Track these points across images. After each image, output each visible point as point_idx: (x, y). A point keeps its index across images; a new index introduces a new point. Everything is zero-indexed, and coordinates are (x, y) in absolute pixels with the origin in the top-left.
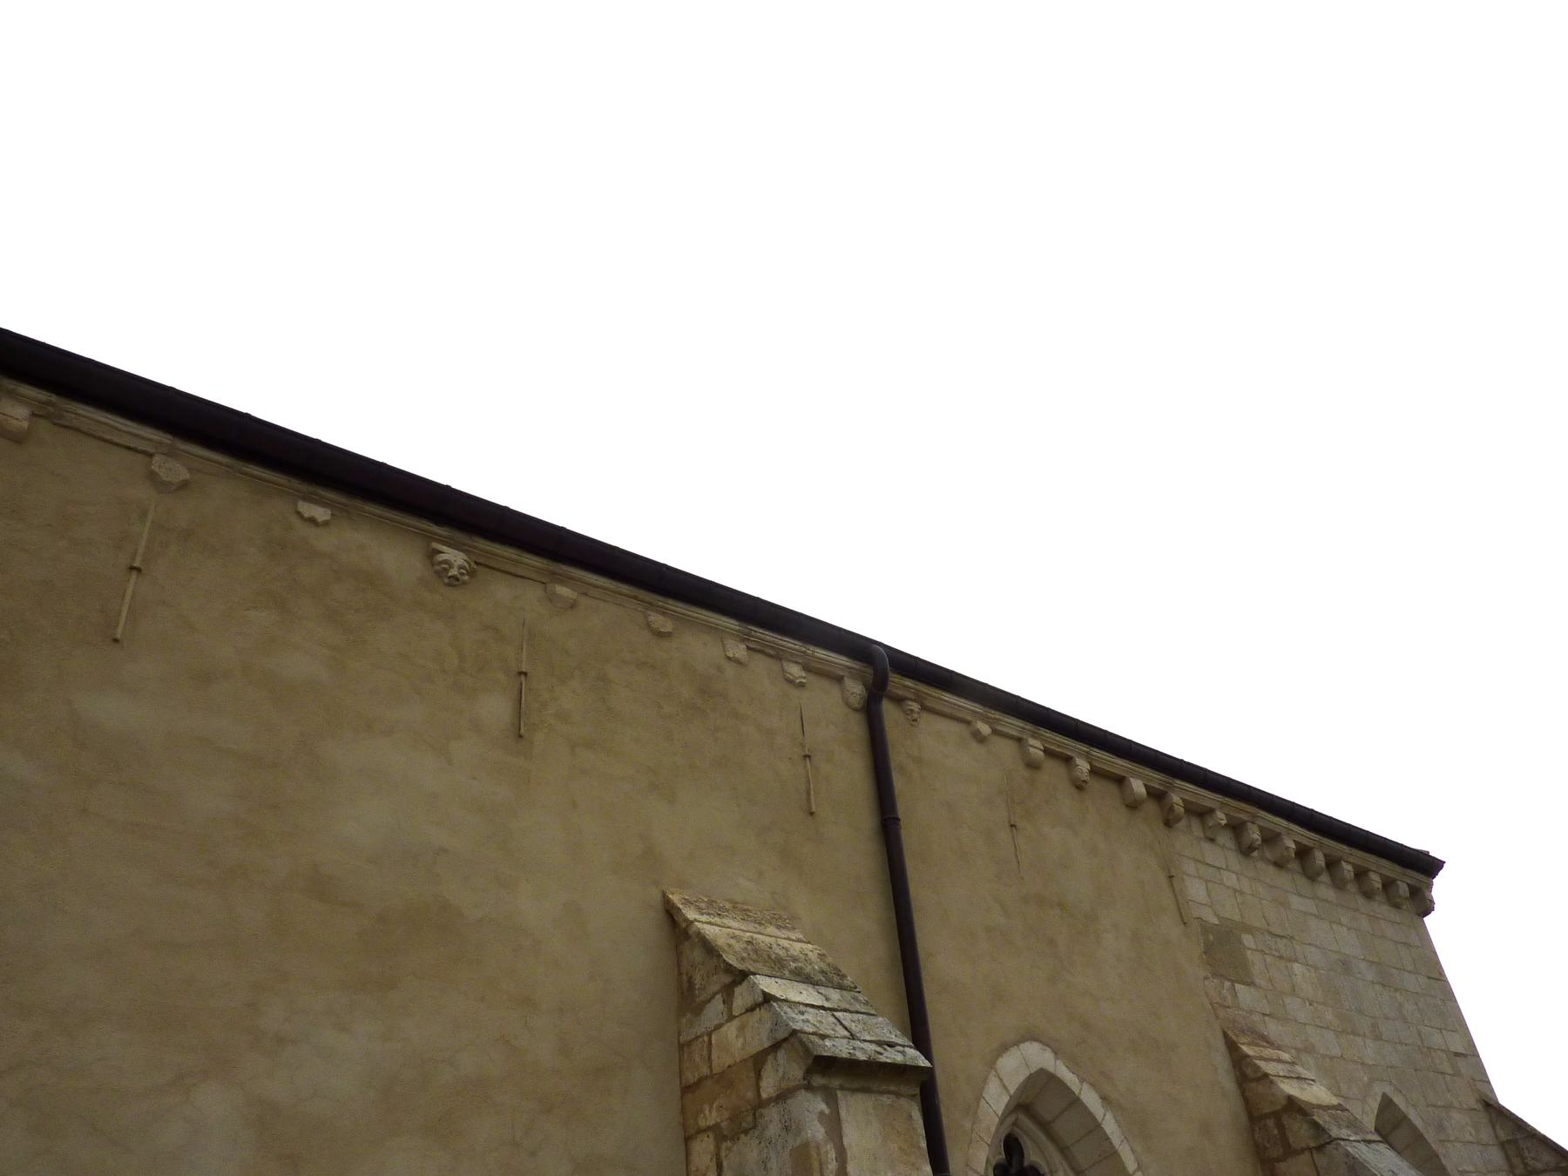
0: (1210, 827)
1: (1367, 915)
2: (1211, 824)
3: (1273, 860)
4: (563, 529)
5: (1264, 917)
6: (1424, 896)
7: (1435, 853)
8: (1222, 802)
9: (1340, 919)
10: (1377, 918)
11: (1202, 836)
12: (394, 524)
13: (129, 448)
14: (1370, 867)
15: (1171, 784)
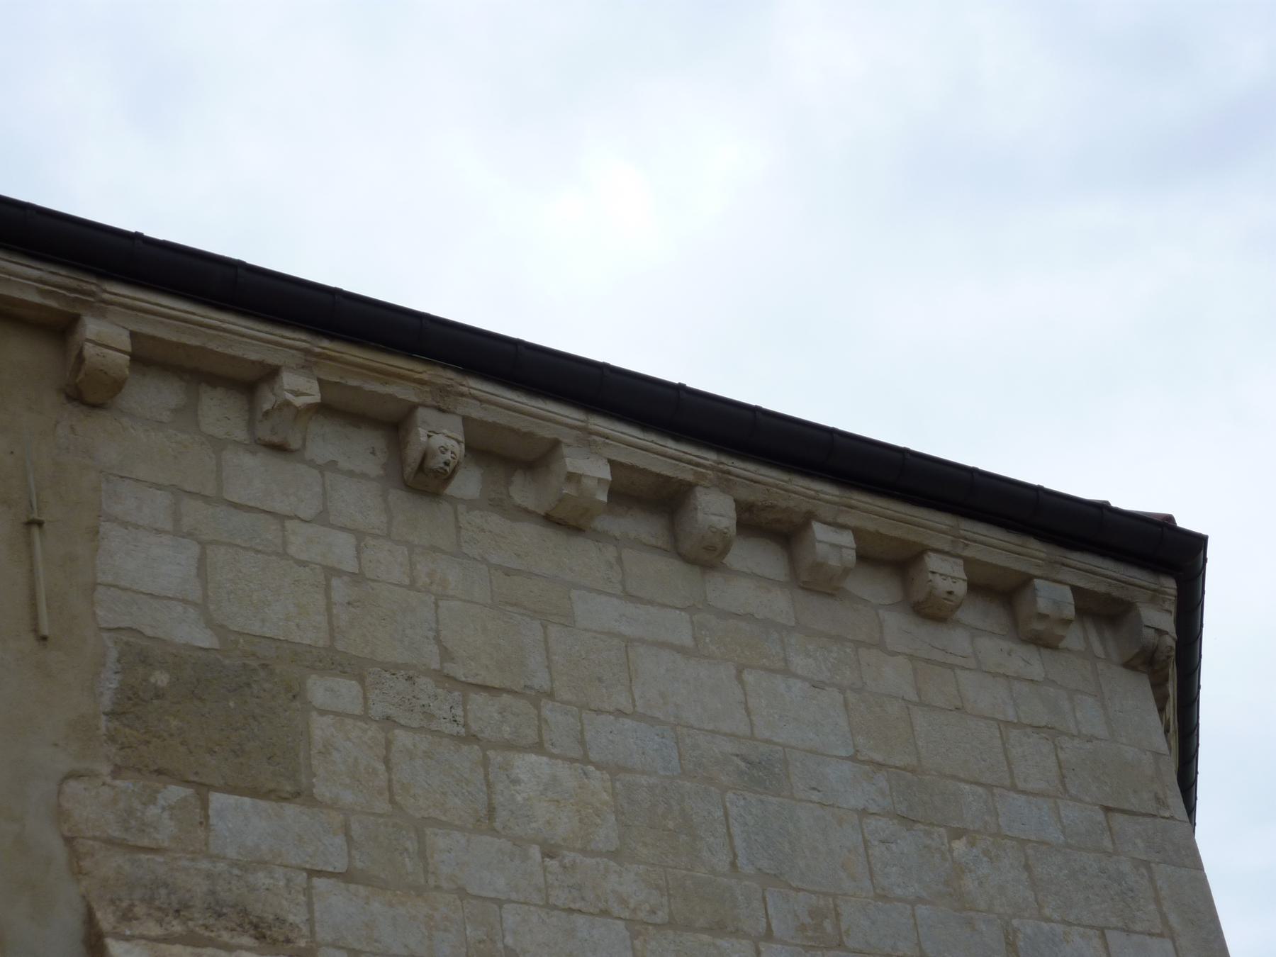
0: (267, 414)
1: (911, 657)
2: (267, 406)
3: (543, 514)
4: (1038, 490)
5: (437, 639)
6: (1139, 616)
7: (1204, 533)
8: (307, 352)
9: (786, 660)
10: (952, 667)
11: (241, 434)
12: (245, 339)
13: (1086, 571)
14: (926, 542)
15: (91, 294)
